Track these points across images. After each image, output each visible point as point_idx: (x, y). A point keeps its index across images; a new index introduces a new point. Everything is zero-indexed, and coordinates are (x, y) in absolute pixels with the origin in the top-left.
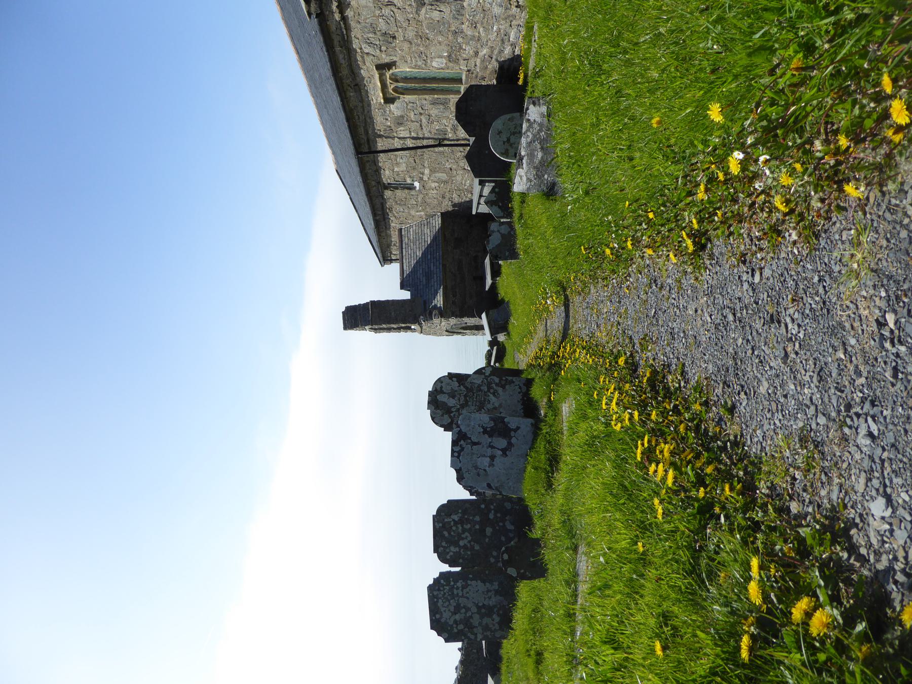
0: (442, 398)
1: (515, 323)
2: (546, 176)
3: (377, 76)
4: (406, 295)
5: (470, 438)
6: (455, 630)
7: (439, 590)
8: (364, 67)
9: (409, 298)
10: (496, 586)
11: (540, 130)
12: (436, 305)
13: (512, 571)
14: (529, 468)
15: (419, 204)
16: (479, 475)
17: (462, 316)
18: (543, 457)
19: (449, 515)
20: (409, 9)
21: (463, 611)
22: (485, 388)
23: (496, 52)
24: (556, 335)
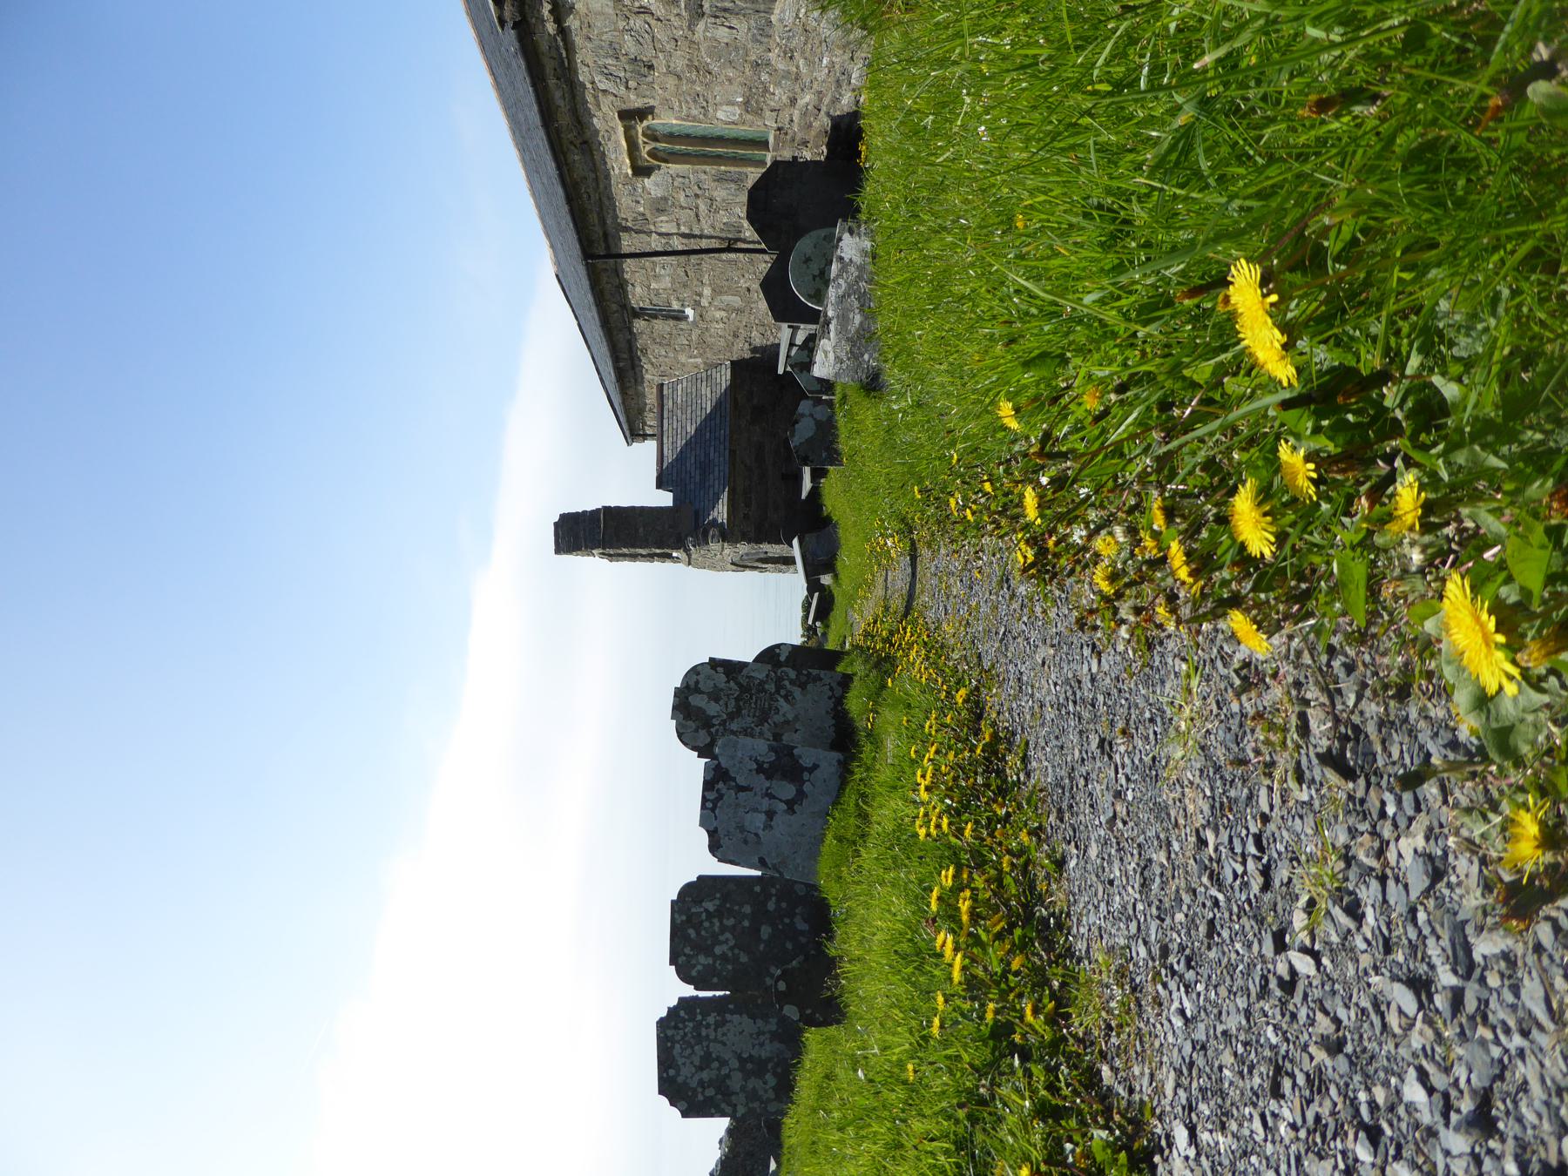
0: (697, 701)
1: (847, 560)
2: (866, 357)
3: (621, 130)
4: (665, 499)
5: (734, 779)
6: (700, 1098)
7: (676, 1027)
12: (715, 520)
13: (791, 1012)
14: (829, 836)
15: (693, 344)
16: (746, 842)
19: (699, 902)
20: (676, 22)
21: (715, 1064)
22: (771, 687)
23: (826, 101)
24: (897, 603)
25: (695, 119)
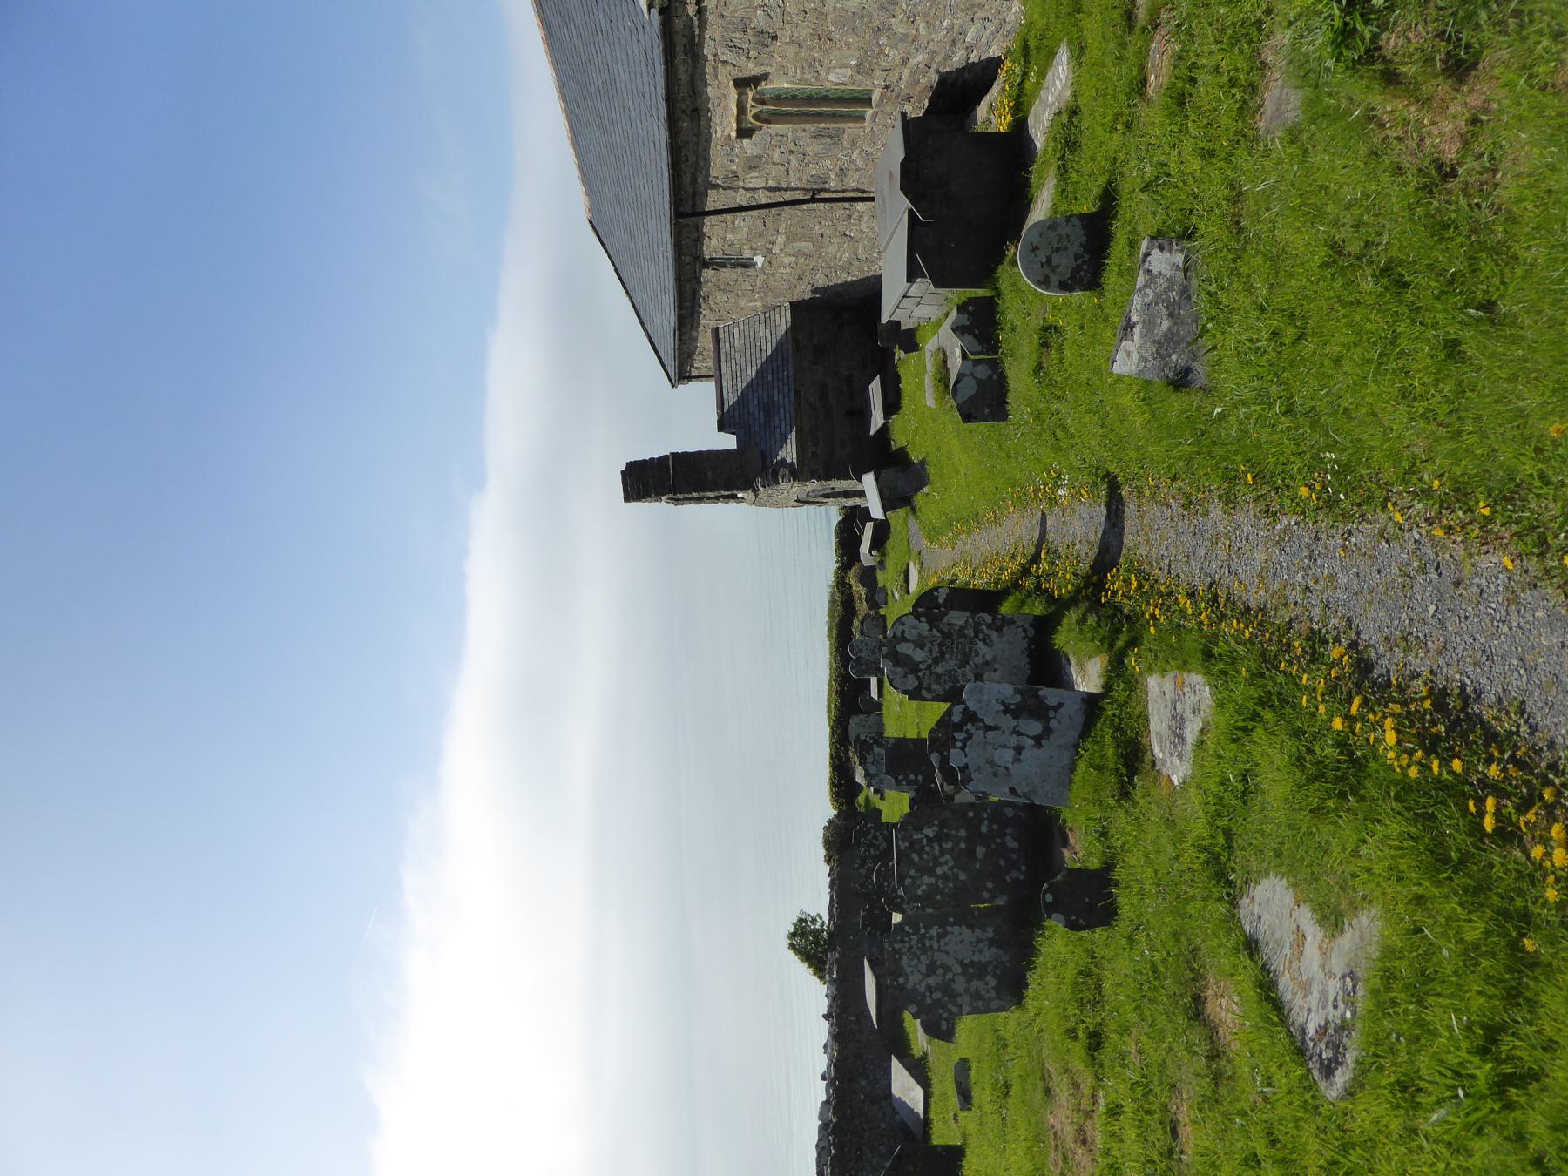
2: (1174, 357)
4: (728, 442)
6: (929, 1001)
7: (902, 941)
8: (715, 83)
9: (735, 447)
10: (990, 933)
11: (1170, 289)
14: (1082, 766)
16: (996, 775)
17: (828, 478)
18: (1110, 751)
19: (919, 829)
21: (940, 971)
23: (938, 59)
25: (806, 82)
